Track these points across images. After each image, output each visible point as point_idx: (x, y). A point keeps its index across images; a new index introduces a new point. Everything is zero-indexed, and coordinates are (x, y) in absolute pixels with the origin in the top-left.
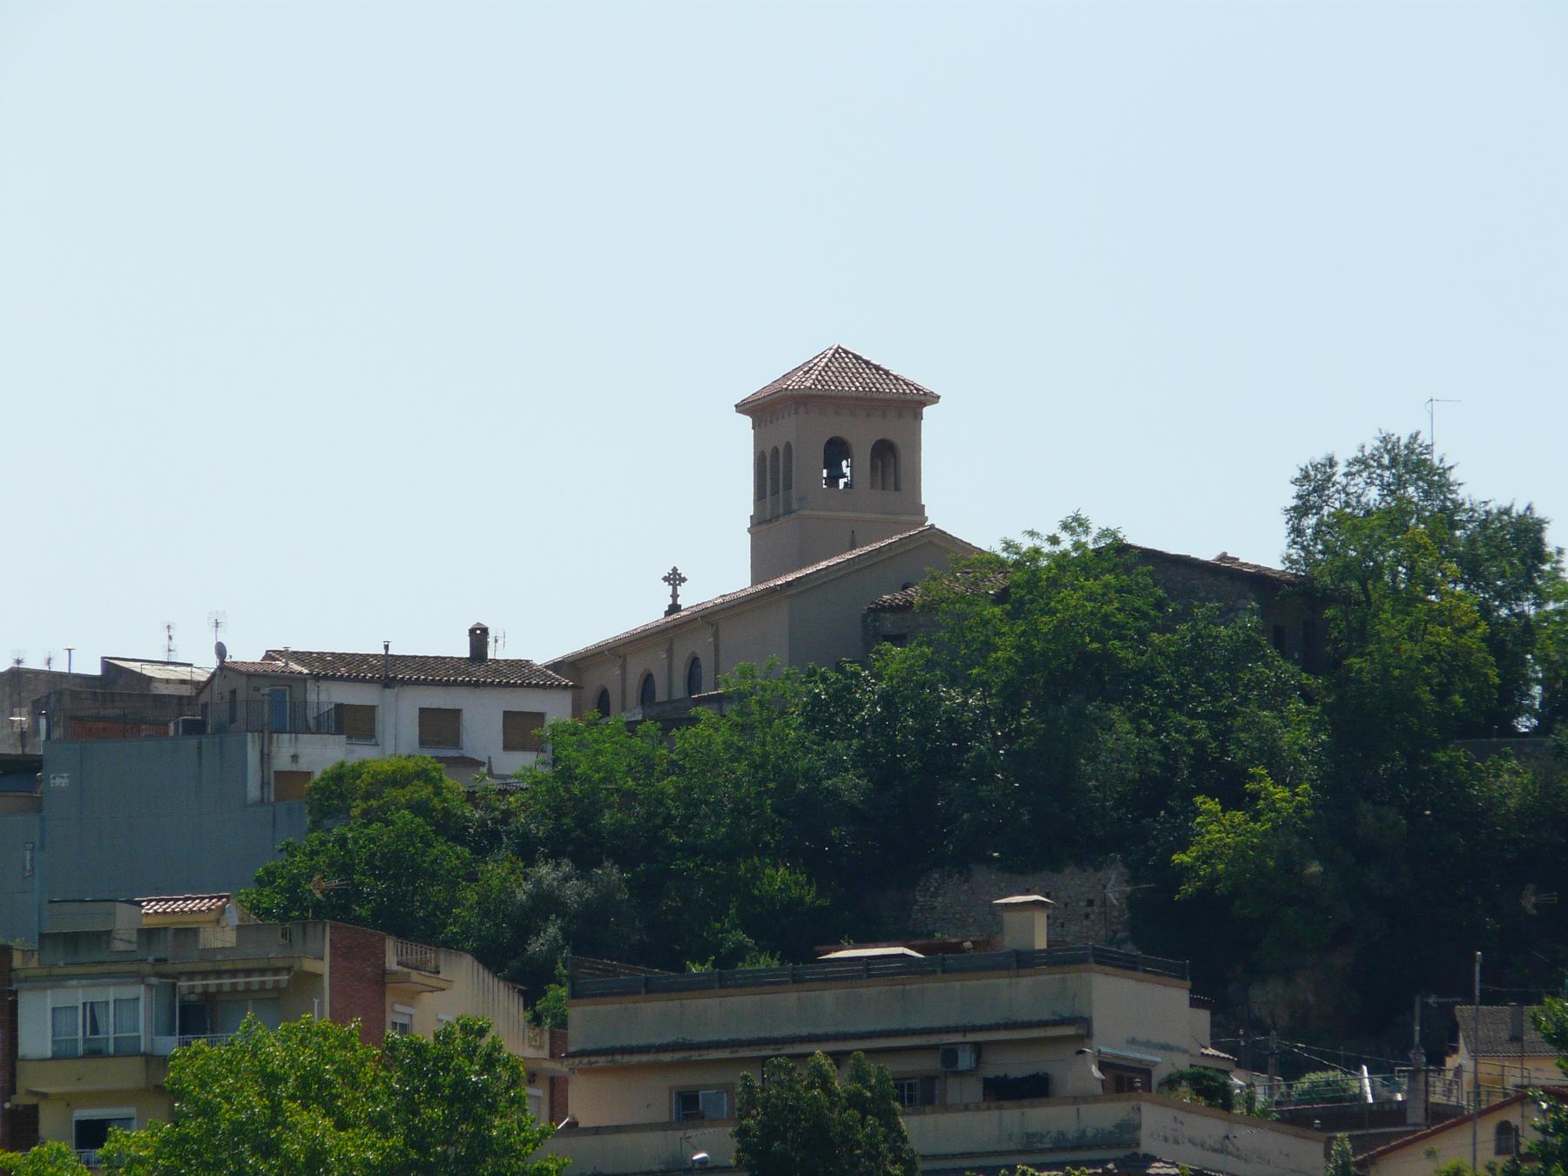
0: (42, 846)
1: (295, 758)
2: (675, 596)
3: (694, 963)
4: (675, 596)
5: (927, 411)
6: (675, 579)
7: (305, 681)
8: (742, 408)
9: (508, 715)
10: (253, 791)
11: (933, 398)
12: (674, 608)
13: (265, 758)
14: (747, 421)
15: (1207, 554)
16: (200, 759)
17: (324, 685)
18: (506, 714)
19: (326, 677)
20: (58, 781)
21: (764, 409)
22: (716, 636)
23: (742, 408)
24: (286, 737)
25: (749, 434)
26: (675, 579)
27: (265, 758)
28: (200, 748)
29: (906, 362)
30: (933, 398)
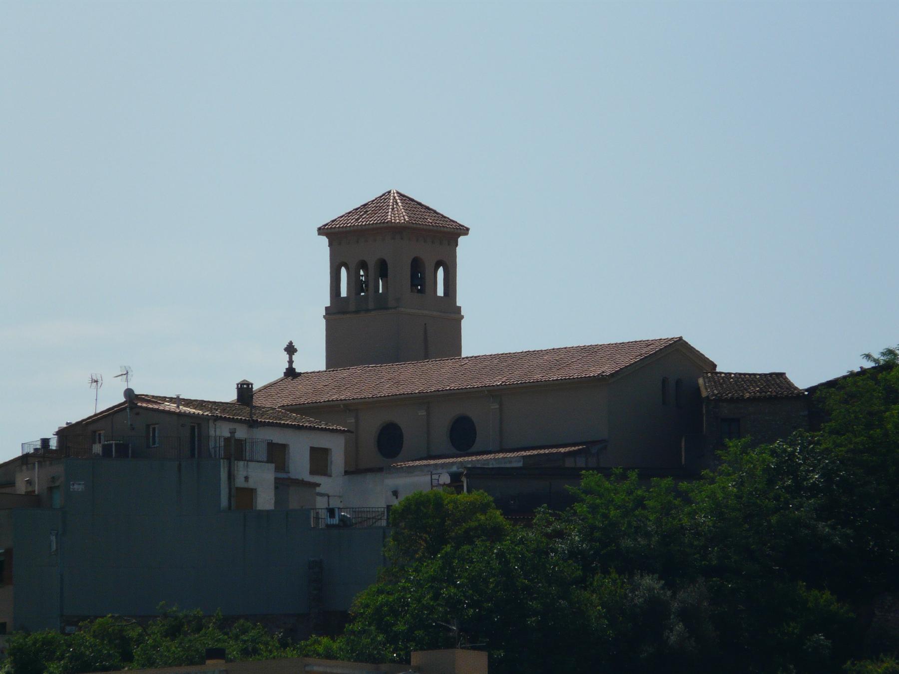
1: (246, 478)
2: (291, 362)
4: (291, 362)
5: (462, 240)
6: (291, 350)
7: (208, 420)
8: (322, 231)
9: (313, 450)
10: (224, 502)
11: (465, 231)
12: (291, 373)
13: (231, 476)
14: (325, 240)
15: (845, 373)
17: (219, 424)
20: (76, 486)
21: (334, 233)
23: (322, 231)
24: (241, 463)
26: (291, 350)
27: (231, 476)
28: (180, 465)
29: (447, 204)
30: (465, 231)
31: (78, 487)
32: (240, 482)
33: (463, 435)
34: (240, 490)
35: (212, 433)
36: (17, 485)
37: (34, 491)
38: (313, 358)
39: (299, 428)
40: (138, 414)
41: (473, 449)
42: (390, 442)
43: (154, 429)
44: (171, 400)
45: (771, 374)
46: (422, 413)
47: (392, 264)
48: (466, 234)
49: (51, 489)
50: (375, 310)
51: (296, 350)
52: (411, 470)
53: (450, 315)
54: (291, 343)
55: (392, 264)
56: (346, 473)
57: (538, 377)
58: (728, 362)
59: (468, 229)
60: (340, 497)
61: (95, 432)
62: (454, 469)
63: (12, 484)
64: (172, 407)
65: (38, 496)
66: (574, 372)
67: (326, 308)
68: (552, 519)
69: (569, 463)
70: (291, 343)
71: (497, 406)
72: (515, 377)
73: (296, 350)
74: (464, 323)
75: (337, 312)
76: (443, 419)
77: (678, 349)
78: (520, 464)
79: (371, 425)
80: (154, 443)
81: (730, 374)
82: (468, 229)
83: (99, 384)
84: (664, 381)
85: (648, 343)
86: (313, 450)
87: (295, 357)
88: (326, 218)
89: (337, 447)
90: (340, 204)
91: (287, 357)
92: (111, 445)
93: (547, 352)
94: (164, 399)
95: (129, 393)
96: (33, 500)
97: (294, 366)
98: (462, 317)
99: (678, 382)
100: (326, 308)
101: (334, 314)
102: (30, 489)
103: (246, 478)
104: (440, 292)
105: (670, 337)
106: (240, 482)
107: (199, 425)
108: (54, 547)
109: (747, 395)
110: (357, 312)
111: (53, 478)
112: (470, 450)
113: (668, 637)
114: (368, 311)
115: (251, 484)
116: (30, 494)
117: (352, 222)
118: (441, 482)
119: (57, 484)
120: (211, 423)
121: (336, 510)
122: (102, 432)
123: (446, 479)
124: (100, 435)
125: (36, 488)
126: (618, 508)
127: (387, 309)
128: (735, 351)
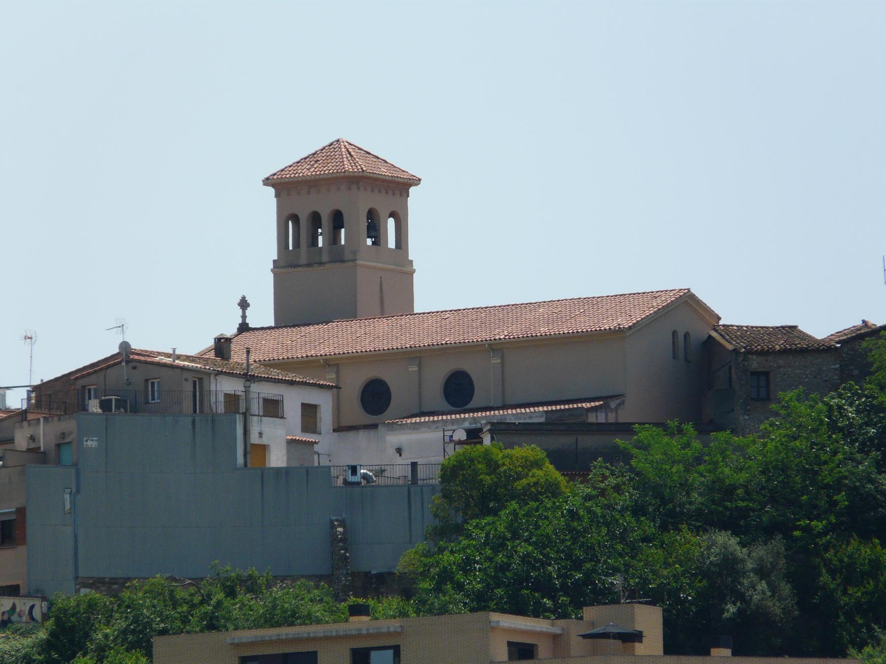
0: (78, 492)
1: (261, 434)
2: (244, 317)
3: (722, 611)
4: (244, 317)
5: (412, 190)
6: (244, 304)
7: (210, 374)
8: (267, 182)
9: (305, 406)
10: (240, 460)
11: (417, 181)
12: (244, 328)
14: (271, 191)
16: (194, 432)
17: (219, 378)
18: (303, 405)
19: (221, 373)
20: (89, 443)
21: (283, 185)
22: (502, 358)
23: (267, 182)
25: (274, 201)
26: (244, 304)
29: (396, 153)
30: (417, 181)
31: (91, 443)
32: (254, 439)
33: (459, 391)
34: (254, 446)
35: (213, 388)
36: (16, 441)
37: (40, 448)
38: (263, 314)
39: (292, 383)
40: (134, 368)
41: (471, 405)
42: (376, 398)
43: (153, 384)
44: (168, 355)
45: (783, 327)
46: (497, 361)
47: (338, 219)
48: (417, 185)
49: (58, 446)
50: (330, 262)
51: (248, 305)
52: (416, 427)
53: (401, 271)
54: (244, 298)
55: (338, 219)
56: (334, 430)
57: (544, 330)
58: (727, 319)
59: (420, 180)
60: (329, 455)
61: (84, 387)
62: (467, 425)
63: (11, 441)
64: (168, 360)
65: (44, 453)
66: (584, 324)
67: (274, 261)
68: (607, 473)
69: (592, 418)
70: (244, 298)
71: (499, 361)
72: (515, 330)
73: (248, 305)
74: (415, 276)
75: (284, 266)
76: (436, 375)
77: (688, 302)
78: (542, 420)
79: (354, 382)
80: (153, 399)
81: (742, 327)
82: (420, 180)
83: (33, 340)
84: (674, 333)
85: (654, 295)
86: (305, 406)
87: (248, 312)
88: (273, 167)
89: (324, 402)
90: (284, 156)
91: (239, 311)
92: (111, 400)
93: (539, 304)
94: (159, 354)
95: (125, 346)
96: (37, 455)
97: (247, 321)
98: (414, 271)
99: (686, 336)
100: (274, 261)
101: (283, 267)
102: (33, 446)
103: (261, 434)
104: (392, 244)
105: (678, 288)
106: (254, 439)
107: (201, 379)
108: (68, 507)
109: (778, 347)
110: (309, 265)
111: (63, 434)
112: (467, 407)
113: (751, 596)
114: (321, 264)
115: (264, 441)
116: (34, 451)
117: (306, 172)
118: (455, 438)
119: (67, 440)
120: (212, 377)
121: (358, 467)
122: (92, 387)
123: (461, 435)
124: (89, 390)
125: (42, 446)
126: (705, 461)
127: (343, 261)
128: (742, 305)
